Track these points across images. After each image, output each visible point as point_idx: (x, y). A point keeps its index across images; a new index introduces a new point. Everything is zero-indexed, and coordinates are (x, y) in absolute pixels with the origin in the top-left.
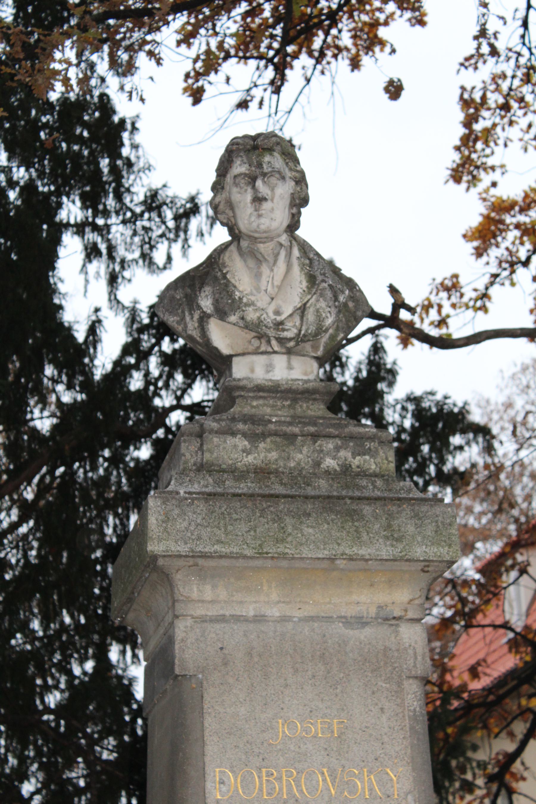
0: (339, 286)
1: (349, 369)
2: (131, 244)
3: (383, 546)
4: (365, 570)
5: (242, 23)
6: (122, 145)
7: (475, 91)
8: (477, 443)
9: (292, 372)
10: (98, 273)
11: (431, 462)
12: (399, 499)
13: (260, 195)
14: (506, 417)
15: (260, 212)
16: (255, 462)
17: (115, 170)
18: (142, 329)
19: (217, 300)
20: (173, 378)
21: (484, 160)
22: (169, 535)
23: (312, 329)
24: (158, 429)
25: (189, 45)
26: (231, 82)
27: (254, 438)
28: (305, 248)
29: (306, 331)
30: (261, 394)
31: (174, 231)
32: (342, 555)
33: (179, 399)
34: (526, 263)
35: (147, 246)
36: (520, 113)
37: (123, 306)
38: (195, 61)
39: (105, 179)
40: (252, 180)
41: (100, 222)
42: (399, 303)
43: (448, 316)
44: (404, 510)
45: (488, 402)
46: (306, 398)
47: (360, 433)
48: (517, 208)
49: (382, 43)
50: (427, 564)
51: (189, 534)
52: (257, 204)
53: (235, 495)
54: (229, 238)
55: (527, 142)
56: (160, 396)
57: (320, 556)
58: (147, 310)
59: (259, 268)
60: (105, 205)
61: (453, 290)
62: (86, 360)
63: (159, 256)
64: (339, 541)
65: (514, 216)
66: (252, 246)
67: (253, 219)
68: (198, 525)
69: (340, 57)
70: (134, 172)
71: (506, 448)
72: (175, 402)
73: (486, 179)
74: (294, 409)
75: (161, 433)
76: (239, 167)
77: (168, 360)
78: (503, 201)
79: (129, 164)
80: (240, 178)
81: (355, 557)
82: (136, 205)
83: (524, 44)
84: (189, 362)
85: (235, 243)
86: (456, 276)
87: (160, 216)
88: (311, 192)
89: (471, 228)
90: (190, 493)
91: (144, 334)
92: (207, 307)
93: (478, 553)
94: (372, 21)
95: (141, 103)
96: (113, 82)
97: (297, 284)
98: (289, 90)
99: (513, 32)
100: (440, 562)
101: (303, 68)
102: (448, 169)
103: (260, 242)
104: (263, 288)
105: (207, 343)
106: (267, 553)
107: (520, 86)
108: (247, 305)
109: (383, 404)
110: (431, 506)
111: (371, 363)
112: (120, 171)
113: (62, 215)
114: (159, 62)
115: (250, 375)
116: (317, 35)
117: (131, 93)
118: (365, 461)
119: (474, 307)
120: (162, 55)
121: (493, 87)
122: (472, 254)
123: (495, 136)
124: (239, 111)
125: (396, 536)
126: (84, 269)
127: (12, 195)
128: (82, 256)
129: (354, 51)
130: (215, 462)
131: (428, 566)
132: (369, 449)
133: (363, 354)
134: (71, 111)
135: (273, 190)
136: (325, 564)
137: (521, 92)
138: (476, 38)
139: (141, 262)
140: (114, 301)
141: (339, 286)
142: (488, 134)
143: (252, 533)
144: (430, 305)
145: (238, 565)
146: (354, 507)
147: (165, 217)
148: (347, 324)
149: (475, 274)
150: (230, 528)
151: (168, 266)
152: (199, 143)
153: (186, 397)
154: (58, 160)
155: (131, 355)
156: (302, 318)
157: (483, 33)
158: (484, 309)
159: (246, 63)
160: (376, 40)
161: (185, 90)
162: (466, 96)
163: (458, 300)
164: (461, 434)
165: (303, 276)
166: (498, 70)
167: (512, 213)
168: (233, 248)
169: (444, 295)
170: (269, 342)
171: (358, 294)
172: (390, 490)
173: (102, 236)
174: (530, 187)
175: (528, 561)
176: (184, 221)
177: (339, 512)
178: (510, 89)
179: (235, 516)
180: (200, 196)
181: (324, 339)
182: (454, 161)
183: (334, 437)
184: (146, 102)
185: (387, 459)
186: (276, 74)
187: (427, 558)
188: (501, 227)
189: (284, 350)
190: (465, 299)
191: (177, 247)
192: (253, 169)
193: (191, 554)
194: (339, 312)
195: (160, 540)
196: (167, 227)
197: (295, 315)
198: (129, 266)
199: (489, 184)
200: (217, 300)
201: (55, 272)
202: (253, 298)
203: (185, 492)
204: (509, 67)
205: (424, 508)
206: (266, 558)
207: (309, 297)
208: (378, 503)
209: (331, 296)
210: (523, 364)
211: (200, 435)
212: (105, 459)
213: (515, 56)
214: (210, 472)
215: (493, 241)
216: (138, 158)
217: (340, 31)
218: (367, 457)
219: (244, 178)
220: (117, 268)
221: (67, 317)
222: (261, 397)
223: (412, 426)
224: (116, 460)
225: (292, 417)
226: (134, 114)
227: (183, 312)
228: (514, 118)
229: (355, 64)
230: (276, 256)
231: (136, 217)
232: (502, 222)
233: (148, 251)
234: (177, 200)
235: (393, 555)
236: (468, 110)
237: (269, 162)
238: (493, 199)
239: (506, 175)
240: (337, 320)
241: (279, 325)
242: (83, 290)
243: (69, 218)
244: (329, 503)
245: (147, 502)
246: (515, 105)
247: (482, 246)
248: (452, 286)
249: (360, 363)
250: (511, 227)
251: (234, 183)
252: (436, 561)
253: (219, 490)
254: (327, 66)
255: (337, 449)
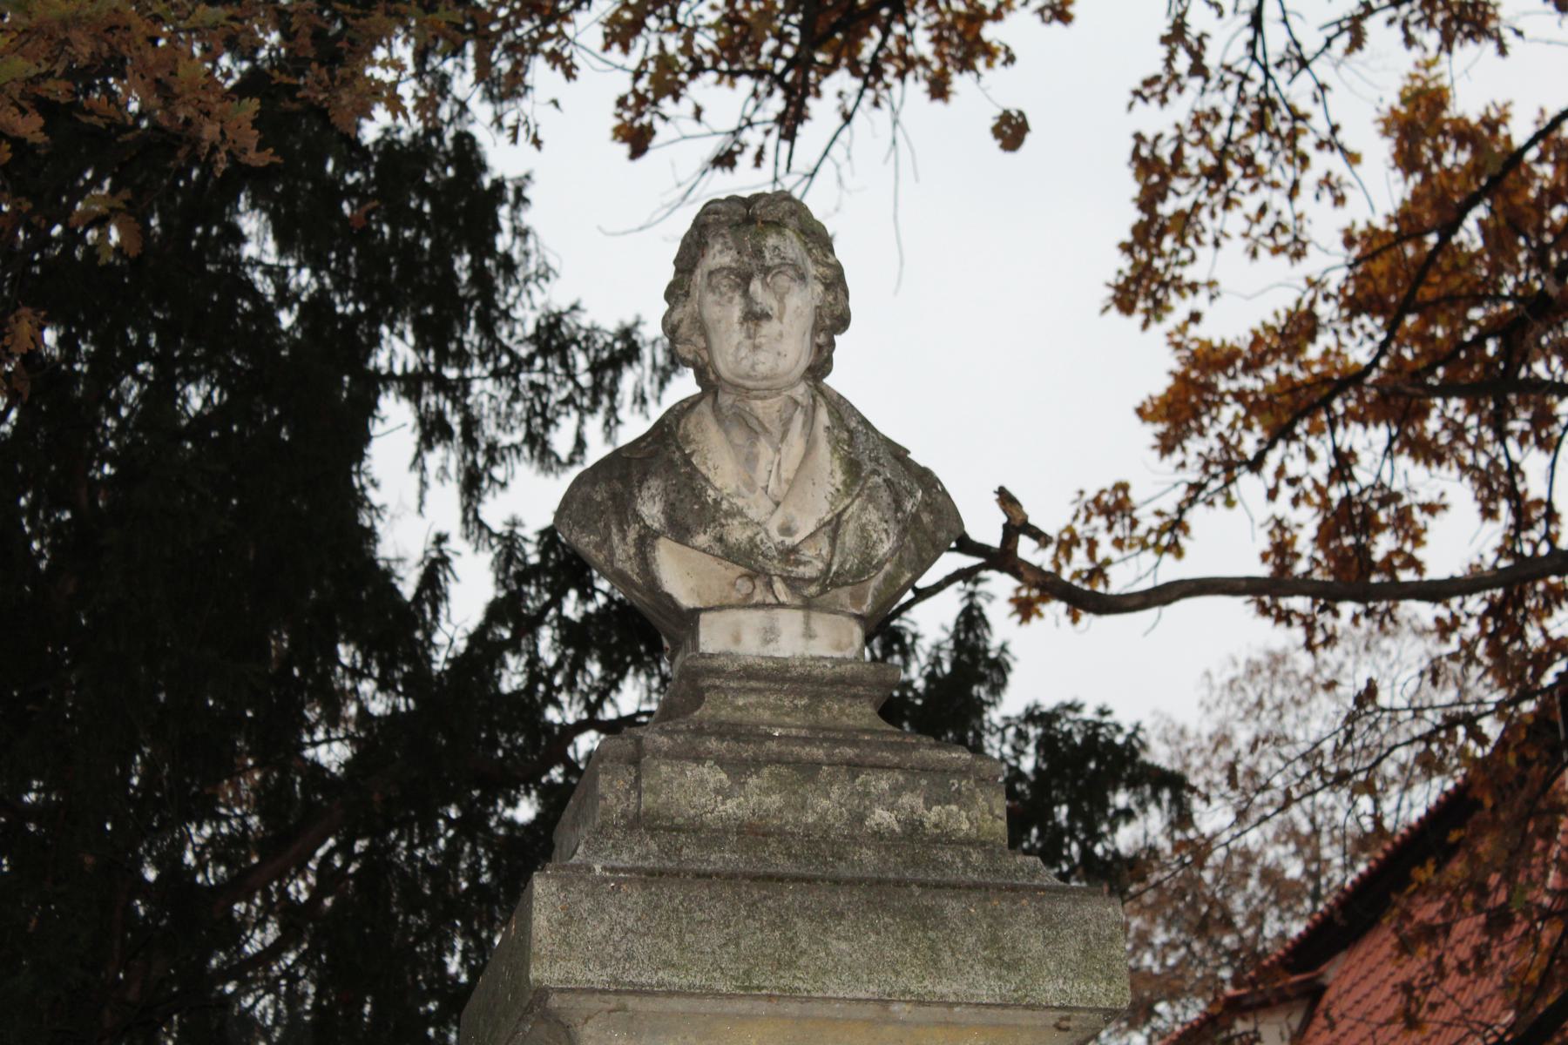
0: (905, 483)
1: (917, 659)
2: (508, 416)
3: (982, 979)
4: (947, 1024)
5: (726, 10)
6: (497, 229)
7: (1161, 143)
8: (1159, 803)
9: (812, 642)
10: (444, 469)
11: (1073, 837)
12: (1014, 888)
13: (757, 309)
14: (1215, 762)
15: (757, 341)
16: (740, 813)
17: (481, 278)
18: (528, 574)
19: (673, 504)
20: (584, 670)
21: (1177, 271)
22: (571, 948)
23: (852, 562)
24: (551, 766)
25: (626, 49)
26: (704, 116)
27: (738, 768)
28: (841, 409)
29: (841, 565)
30: (753, 684)
31: (589, 393)
32: (903, 993)
33: (592, 708)
34: (1256, 465)
35: (539, 420)
36: (1245, 185)
37: (489, 530)
38: (638, 75)
39: (462, 292)
40: (743, 280)
41: (451, 373)
42: (1017, 523)
43: (1108, 562)
44: (1022, 909)
45: (1182, 732)
46: (838, 693)
47: (940, 761)
48: (1239, 363)
49: (989, 52)
50: (1066, 1014)
51: (611, 949)
52: (751, 325)
53: (699, 875)
54: (698, 390)
55: (1257, 241)
56: (558, 705)
57: (862, 995)
58: (535, 538)
59: (753, 444)
60: (460, 342)
61: (1119, 514)
62: (419, 635)
63: (561, 440)
64: (898, 967)
65: (1234, 377)
66: (740, 404)
67: (743, 353)
68: (627, 931)
69: (910, 77)
70: (517, 282)
71: (1212, 818)
72: (585, 716)
73: (1180, 307)
74: (815, 713)
75: (556, 774)
76: (719, 256)
77: (575, 637)
78: (1214, 350)
79: (508, 265)
80: (719, 277)
81: (927, 998)
82: (520, 342)
83: (1254, 58)
84: (614, 639)
85: (709, 399)
86: (1123, 487)
87: (564, 363)
88: (857, 304)
89: (1151, 398)
90: (614, 870)
91: (529, 584)
92: (652, 517)
93: (1159, 1023)
94: (972, 12)
95: (533, 148)
96: (482, 111)
97: (826, 475)
98: (811, 135)
99: (1234, 36)
100: (1091, 1010)
101: (840, 94)
102: (1108, 285)
103: (756, 398)
104: (762, 484)
105: (652, 584)
106: (759, 988)
107: (1246, 136)
108: (730, 514)
109: (982, 727)
110: (1075, 902)
111: (959, 645)
112: (491, 280)
113: (380, 360)
114: (569, 72)
115: (733, 649)
116: (868, 35)
117: (515, 129)
118: (949, 815)
119: (1156, 545)
120: (577, 60)
121: (1194, 136)
122: (1154, 447)
123: (1198, 228)
124: (718, 171)
125: (1006, 958)
126: (418, 462)
127: (286, 319)
128: (415, 437)
129: (936, 65)
130: (663, 812)
131: (1068, 1019)
132: (958, 791)
133: (944, 628)
134: (401, 163)
135: (781, 300)
136: (871, 1011)
137: (1247, 147)
138: (1165, 40)
139: (525, 450)
140: (473, 522)
141: (905, 483)
142: (1184, 222)
143: (732, 948)
144: (1074, 541)
145: (702, 1009)
146: (927, 901)
147: (574, 366)
148: (919, 556)
149: (1156, 483)
150: (689, 938)
151: (577, 458)
152: (641, 229)
153: (607, 706)
154: (374, 256)
155: (505, 625)
156: (833, 540)
157: (1177, 33)
158: (1176, 549)
159: (732, 85)
160: (978, 47)
161: (617, 132)
162: (1145, 152)
163: (1127, 532)
164: (1127, 788)
165: (837, 463)
166: (1205, 105)
167: (1231, 372)
168: (705, 407)
169: (1100, 522)
170: (769, 586)
171: (940, 499)
172: (997, 871)
173: (455, 401)
174: (1263, 324)
175: (1255, 1031)
176: (609, 374)
177: (900, 910)
178: (1228, 141)
179: (698, 915)
180: (641, 328)
181: (875, 582)
182: (1120, 272)
183: (891, 768)
184: (544, 146)
185: (991, 812)
186: (788, 106)
187: (1066, 1003)
188: (1210, 397)
189: (798, 602)
190: (1140, 531)
191: (594, 425)
192: (746, 259)
193: (613, 987)
194: (904, 531)
195: (553, 960)
196: (577, 385)
197: (820, 534)
198: (503, 458)
199: (1186, 316)
200: (673, 504)
201: (364, 465)
202: (740, 503)
203: (604, 868)
204: (1225, 99)
205: (1062, 907)
206: (757, 997)
207: (847, 501)
208: (975, 896)
209: (889, 500)
210: (1249, 661)
211: (635, 761)
212: (450, 823)
213: (1236, 80)
214: (652, 831)
215: (1193, 424)
216: (526, 254)
217: (910, 29)
218: (954, 808)
219: (727, 277)
220: (481, 461)
221: (385, 550)
222: (753, 690)
223: (1037, 770)
224: (472, 825)
225: (811, 728)
226: (520, 172)
227: (607, 527)
228: (1233, 195)
229: (939, 89)
230: (786, 424)
231: (520, 364)
232: (1212, 388)
233: (541, 431)
234: (597, 335)
235: (1002, 996)
236: (1148, 176)
237: (776, 248)
238: (1194, 346)
239: (1218, 302)
240: (899, 548)
241: (789, 554)
242: (415, 502)
243: (391, 364)
244: (880, 894)
245: (532, 886)
246: (1235, 171)
247: (1172, 433)
248: (1115, 506)
249: (938, 647)
250: (1229, 399)
251: (709, 284)
252: (1083, 1009)
253: (669, 864)
254: (885, 93)
255: (897, 790)
